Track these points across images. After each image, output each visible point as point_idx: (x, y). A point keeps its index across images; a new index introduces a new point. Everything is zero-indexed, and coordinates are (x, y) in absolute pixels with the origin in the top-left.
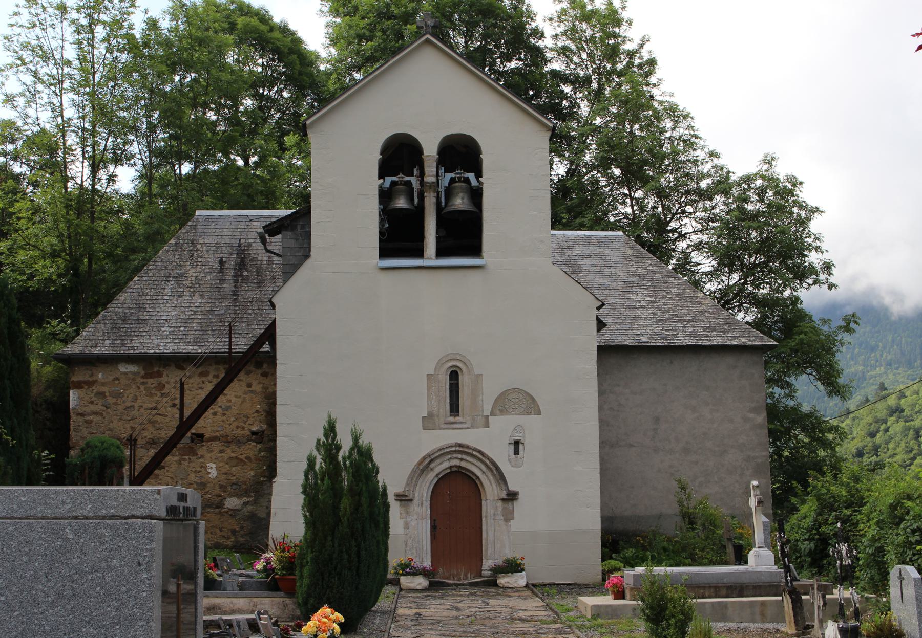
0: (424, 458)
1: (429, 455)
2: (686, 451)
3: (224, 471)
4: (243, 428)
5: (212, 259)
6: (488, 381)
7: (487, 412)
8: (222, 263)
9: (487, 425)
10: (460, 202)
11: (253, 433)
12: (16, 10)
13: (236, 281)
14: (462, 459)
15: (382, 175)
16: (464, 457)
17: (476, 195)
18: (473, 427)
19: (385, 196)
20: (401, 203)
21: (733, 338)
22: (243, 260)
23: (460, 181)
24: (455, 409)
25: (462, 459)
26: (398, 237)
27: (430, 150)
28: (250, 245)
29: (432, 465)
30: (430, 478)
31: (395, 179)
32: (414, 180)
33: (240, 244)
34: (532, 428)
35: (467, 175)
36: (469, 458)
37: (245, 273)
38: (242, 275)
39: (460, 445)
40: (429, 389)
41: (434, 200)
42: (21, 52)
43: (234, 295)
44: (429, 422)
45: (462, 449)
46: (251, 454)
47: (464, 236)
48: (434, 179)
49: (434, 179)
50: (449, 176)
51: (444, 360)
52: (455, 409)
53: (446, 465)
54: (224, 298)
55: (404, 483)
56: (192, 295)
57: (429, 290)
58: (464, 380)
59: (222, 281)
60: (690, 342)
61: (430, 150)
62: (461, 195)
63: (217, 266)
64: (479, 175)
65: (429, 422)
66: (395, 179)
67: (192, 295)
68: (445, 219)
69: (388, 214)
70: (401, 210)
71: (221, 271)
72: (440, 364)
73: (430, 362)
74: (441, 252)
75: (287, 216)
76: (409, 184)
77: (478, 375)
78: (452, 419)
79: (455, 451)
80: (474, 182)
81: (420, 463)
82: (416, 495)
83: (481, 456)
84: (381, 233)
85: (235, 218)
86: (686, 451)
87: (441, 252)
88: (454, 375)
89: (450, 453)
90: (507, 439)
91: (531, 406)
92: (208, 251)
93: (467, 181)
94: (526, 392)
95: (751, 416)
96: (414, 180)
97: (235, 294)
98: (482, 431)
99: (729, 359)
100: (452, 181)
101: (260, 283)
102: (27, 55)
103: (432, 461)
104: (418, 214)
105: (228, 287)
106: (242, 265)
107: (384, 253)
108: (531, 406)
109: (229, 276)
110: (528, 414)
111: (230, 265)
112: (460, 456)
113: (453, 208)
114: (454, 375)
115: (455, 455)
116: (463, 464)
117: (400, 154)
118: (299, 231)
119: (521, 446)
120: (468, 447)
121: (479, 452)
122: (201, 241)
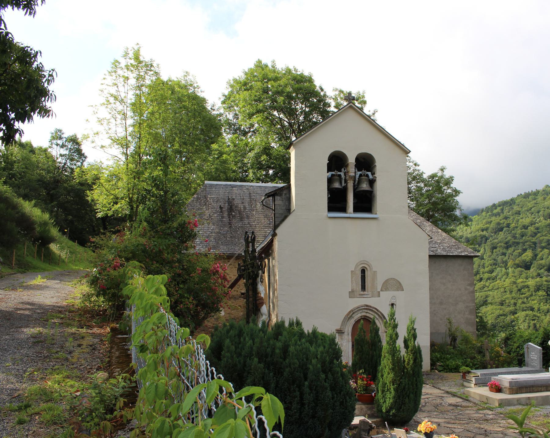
0: (350, 312)
1: (352, 311)
2: (441, 303)
3: (228, 312)
4: (237, 291)
5: (216, 205)
6: (380, 274)
7: (379, 290)
8: (221, 208)
9: (379, 296)
10: (365, 186)
11: (242, 294)
12: (105, 77)
13: (229, 217)
14: (367, 313)
15: (329, 170)
16: (368, 311)
17: (372, 182)
18: (372, 297)
19: (330, 181)
20: (337, 185)
21: (461, 252)
22: (231, 207)
23: (364, 176)
24: (363, 288)
25: (367, 313)
26: (336, 202)
27: (352, 160)
28: (233, 199)
29: (353, 315)
30: (352, 321)
31: (333, 173)
32: (342, 174)
33: (229, 199)
34: (400, 297)
35: (367, 173)
36: (370, 312)
37: (233, 214)
38: (232, 215)
39: (367, 306)
40: (352, 278)
41: (352, 184)
42: (109, 98)
43: (230, 224)
44: (352, 294)
45: (368, 308)
46: (241, 304)
47: (365, 203)
48: (354, 174)
49: (354, 174)
50: (359, 173)
51: (359, 264)
52: (363, 288)
53: (359, 315)
54: (225, 226)
55: (340, 324)
56: (209, 224)
57: (350, 228)
58: (368, 274)
59: (223, 217)
60: (445, 253)
61: (352, 160)
62: (366, 182)
63: (219, 209)
64: (373, 174)
65: (352, 294)
66: (333, 173)
67: (209, 224)
68: (358, 195)
69: (331, 190)
70: (337, 189)
71: (221, 212)
72: (357, 266)
73: (352, 266)
74: (356, 210)
75: (282, 187)
76: (340, 176)
77: (375, 272)
78: (362, 293)
79: (364, 309)
80: (371, 177)
81: (348, 314)
82: (346, 330)
83: (376, 311)
84: (328, 198)
85: (224, 185)
86: (441, 303)
87: (356, 210)
88: (363, 271)
89: (361, 309)
90: (389, 303)
91: (399, 287)
92: (213, 201)
93: (367, 176)
94: (398, 281)
95: (468, 287)
96: (342, 174)
97: (230, 224)
98: (376, 299)
99: (459, 261)
100: (361, 175)
101: (242, 219)
102: (112, 100)
103: (353, 313)
104: (343, 192)
105: (226, 220)
106: (231, 209)
107: (331, 209)
108: (399, 287)
109: (226, 214)
110: (398, 291)
111: (226, 209)
112: (366, 311)
113: (362, 189)
114: (363, 271)
115: (364, 311)
116: (368, 315)
117: (337, 161)
118: (284, 196)
119: (394, 306)
120: (370, 307)
121: (376, 309)
122: (209, 196)
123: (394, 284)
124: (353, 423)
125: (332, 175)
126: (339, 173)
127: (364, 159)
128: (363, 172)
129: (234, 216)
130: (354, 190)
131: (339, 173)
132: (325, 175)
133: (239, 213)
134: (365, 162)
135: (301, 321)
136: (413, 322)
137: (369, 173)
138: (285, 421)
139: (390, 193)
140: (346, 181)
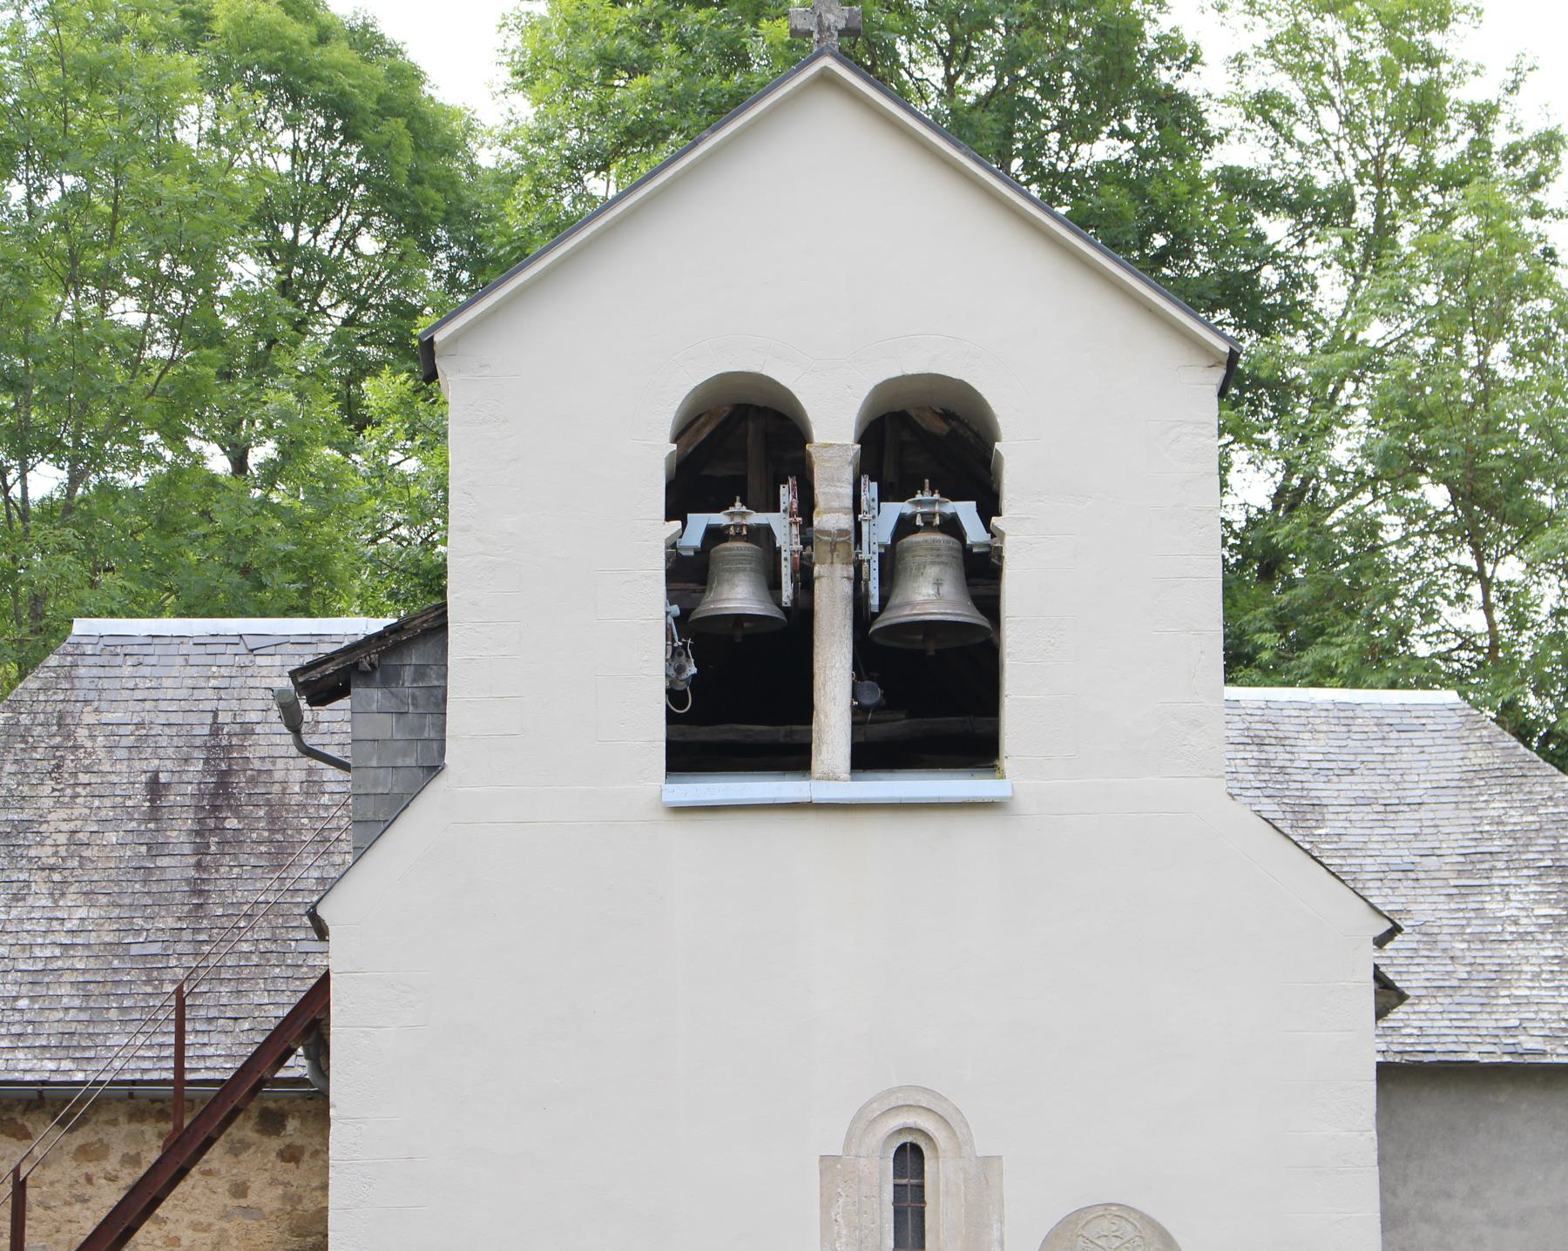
5: (127, 775)
8: (155, 788)
10: (931, 596)
13: (201, 850)
15: (677, 508)
19: (688, 574)
20: (738, 596)
22: (223, 782)
23: (928, 526)
26: (734, 703)
27: (834, 430)
28: (247, 730)
31: (720, 519)
32: (782, 526)
33: (216, 729)
35: (951, 507)
37: (232, 823)
41: (847, 588)
47: (939, 702)
50: (894, 510)
51: (878, 1108)
54: (162, 902)
56: (58, 892)
57: (833, 867)
58: (938, 1174)
61: (834, 430)
62: (933, 571)
63: (140, 800)
66: (720, 519)
67: (58, 892)
68: (883, 654)
70: (739, 619)
72: (862, 1122)
74: (866, 758)
76: (763, 535)
77: (989, 1162)
80: (975, 532)
87: (866, 758)
88: (909, 1158)
93: (952, 526)
94: (1152, 1223)
96: (782, 526)
97: (197, 890)
100: (905, 526)
101: (280, 856)
104: (793, 634)
105: (177, 867)
107: (684, 758)
109: (179, 832)
114: (909, 1158)
117: (735, 446)
122: (89, 718)
125: (715, 535)
126: (757, 518)
127: (947, 415)
128: (927, 502)
129: (232, 842)
130: (862, 617)
131: (757, 518)
132: (647, 534)
133: (272, 819)
137: (966, 511)
140: (805, 580)
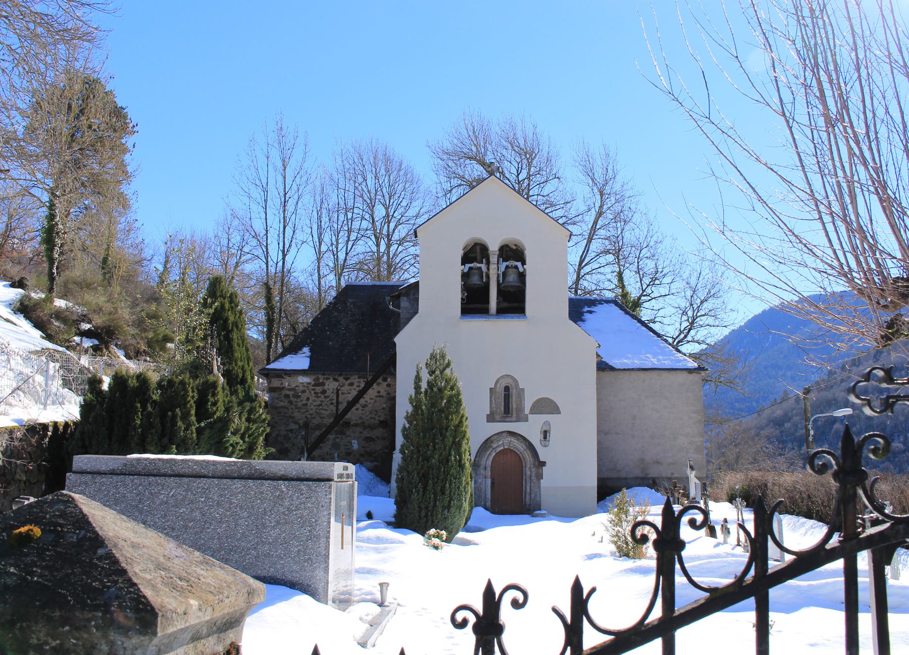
15: (463, 263)
19: (465, 276)
26: (474, 302)
44: (491, 418)
47: (513, 302)
58: (513, 392)
65: (491, 418)
76: (480, 268)
80: (521, 270)
93: (516, 267)
100: (507, 267)
123: (546, 406)
124: (770, 571)
125: (470, 268)
132: (457, 269)
134: (513, 253)
135: (461, 253)
136: (475, 544)
138: (97, 541)
139: (545, 293)
